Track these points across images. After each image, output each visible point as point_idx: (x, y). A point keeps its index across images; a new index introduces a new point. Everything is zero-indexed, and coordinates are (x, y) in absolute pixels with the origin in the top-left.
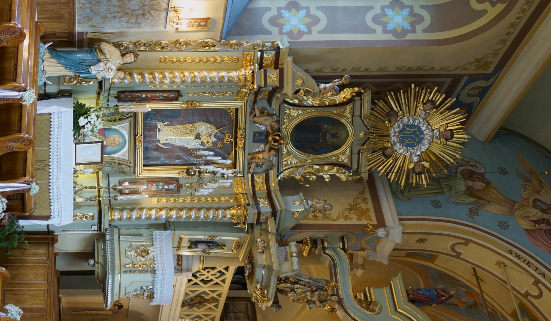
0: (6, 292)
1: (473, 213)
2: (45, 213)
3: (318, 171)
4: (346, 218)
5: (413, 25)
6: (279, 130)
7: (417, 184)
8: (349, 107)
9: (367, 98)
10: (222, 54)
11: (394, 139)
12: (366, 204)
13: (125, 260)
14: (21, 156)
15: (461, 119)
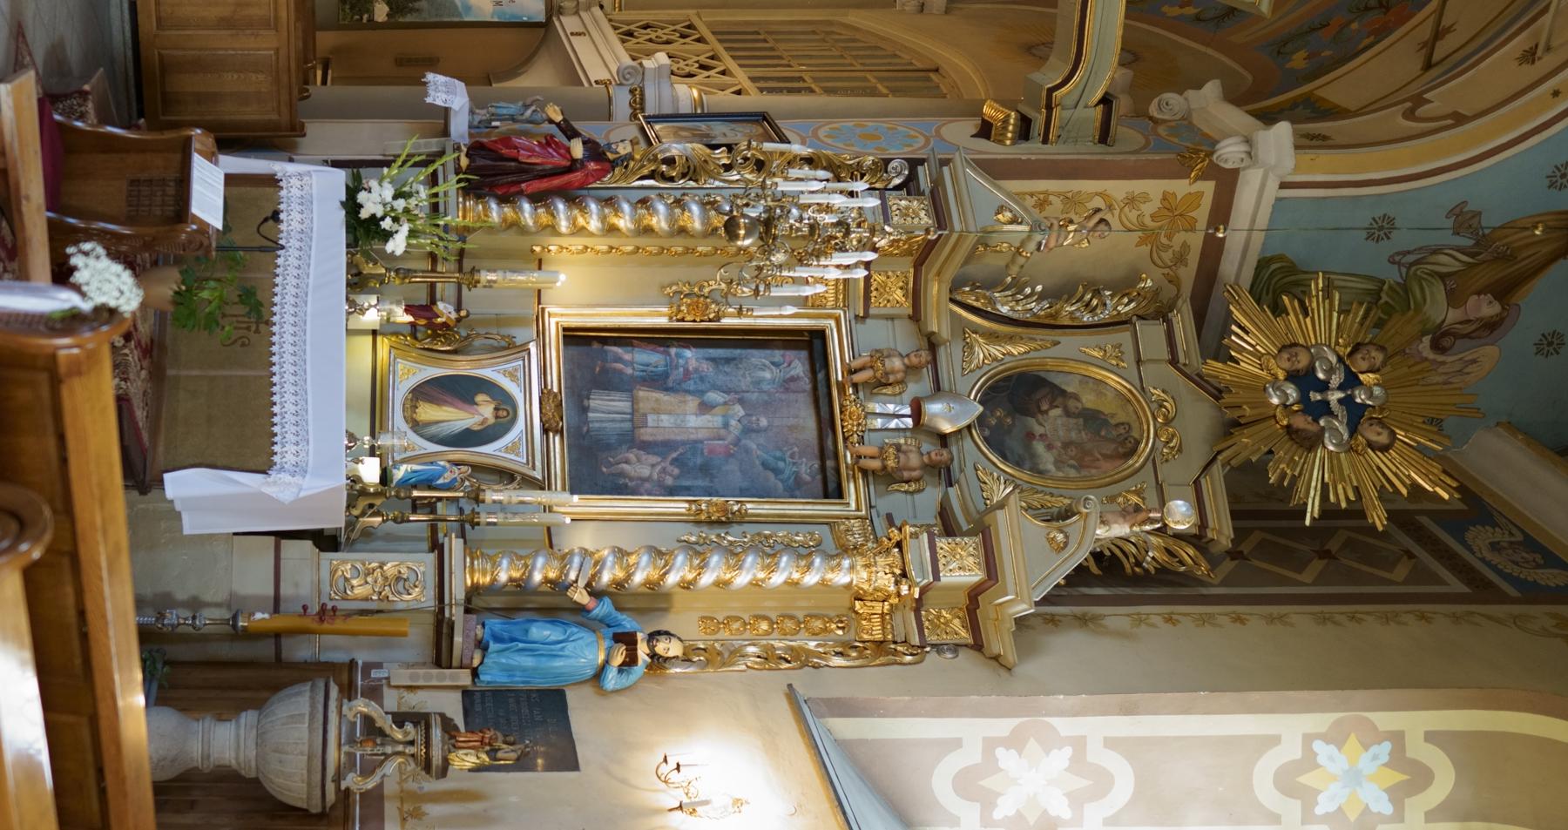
0: (807, 468)
5: (990, 764)
14: (152, 700)
15: (1365, 317)
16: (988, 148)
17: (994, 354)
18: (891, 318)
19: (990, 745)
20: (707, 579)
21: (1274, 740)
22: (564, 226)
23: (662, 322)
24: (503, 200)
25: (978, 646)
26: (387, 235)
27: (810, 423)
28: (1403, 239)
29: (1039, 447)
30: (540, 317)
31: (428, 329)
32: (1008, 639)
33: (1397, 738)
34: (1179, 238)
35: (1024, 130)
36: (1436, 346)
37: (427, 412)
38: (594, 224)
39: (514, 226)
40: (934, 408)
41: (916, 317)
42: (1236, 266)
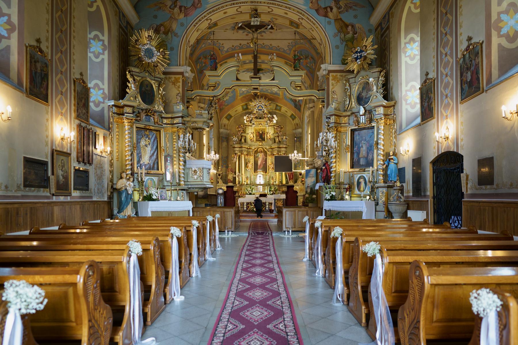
0: (370, 131)
1: (178, 37)
2: (187, 213)
3: (161, 95)
4: (179, 87)
5: (100, 40)
6: (146, 110)
7: (168, 56)
8: (136, 78)
9: (133, 69)
10: (115, 131)
11: (150, 61)
16: (325, 107)
17: (354, 103)
18: (349, 119)
19: (407, 104)
21: (406, 62)
22: (335, 169)
23: (350, 154)
25: (394, 106)
26: (332, 195)
28: (339, 43)
29: (367, 96)
30: (349, 172)
32: (391, 102)
33: (405, 43)
34: (338, 77)
35: (323, 101)
36: (356, 34)
37: (362, 189)
38: (334, 165)
39: (335, 176)
40: (361, 114)
41: (349, 116)
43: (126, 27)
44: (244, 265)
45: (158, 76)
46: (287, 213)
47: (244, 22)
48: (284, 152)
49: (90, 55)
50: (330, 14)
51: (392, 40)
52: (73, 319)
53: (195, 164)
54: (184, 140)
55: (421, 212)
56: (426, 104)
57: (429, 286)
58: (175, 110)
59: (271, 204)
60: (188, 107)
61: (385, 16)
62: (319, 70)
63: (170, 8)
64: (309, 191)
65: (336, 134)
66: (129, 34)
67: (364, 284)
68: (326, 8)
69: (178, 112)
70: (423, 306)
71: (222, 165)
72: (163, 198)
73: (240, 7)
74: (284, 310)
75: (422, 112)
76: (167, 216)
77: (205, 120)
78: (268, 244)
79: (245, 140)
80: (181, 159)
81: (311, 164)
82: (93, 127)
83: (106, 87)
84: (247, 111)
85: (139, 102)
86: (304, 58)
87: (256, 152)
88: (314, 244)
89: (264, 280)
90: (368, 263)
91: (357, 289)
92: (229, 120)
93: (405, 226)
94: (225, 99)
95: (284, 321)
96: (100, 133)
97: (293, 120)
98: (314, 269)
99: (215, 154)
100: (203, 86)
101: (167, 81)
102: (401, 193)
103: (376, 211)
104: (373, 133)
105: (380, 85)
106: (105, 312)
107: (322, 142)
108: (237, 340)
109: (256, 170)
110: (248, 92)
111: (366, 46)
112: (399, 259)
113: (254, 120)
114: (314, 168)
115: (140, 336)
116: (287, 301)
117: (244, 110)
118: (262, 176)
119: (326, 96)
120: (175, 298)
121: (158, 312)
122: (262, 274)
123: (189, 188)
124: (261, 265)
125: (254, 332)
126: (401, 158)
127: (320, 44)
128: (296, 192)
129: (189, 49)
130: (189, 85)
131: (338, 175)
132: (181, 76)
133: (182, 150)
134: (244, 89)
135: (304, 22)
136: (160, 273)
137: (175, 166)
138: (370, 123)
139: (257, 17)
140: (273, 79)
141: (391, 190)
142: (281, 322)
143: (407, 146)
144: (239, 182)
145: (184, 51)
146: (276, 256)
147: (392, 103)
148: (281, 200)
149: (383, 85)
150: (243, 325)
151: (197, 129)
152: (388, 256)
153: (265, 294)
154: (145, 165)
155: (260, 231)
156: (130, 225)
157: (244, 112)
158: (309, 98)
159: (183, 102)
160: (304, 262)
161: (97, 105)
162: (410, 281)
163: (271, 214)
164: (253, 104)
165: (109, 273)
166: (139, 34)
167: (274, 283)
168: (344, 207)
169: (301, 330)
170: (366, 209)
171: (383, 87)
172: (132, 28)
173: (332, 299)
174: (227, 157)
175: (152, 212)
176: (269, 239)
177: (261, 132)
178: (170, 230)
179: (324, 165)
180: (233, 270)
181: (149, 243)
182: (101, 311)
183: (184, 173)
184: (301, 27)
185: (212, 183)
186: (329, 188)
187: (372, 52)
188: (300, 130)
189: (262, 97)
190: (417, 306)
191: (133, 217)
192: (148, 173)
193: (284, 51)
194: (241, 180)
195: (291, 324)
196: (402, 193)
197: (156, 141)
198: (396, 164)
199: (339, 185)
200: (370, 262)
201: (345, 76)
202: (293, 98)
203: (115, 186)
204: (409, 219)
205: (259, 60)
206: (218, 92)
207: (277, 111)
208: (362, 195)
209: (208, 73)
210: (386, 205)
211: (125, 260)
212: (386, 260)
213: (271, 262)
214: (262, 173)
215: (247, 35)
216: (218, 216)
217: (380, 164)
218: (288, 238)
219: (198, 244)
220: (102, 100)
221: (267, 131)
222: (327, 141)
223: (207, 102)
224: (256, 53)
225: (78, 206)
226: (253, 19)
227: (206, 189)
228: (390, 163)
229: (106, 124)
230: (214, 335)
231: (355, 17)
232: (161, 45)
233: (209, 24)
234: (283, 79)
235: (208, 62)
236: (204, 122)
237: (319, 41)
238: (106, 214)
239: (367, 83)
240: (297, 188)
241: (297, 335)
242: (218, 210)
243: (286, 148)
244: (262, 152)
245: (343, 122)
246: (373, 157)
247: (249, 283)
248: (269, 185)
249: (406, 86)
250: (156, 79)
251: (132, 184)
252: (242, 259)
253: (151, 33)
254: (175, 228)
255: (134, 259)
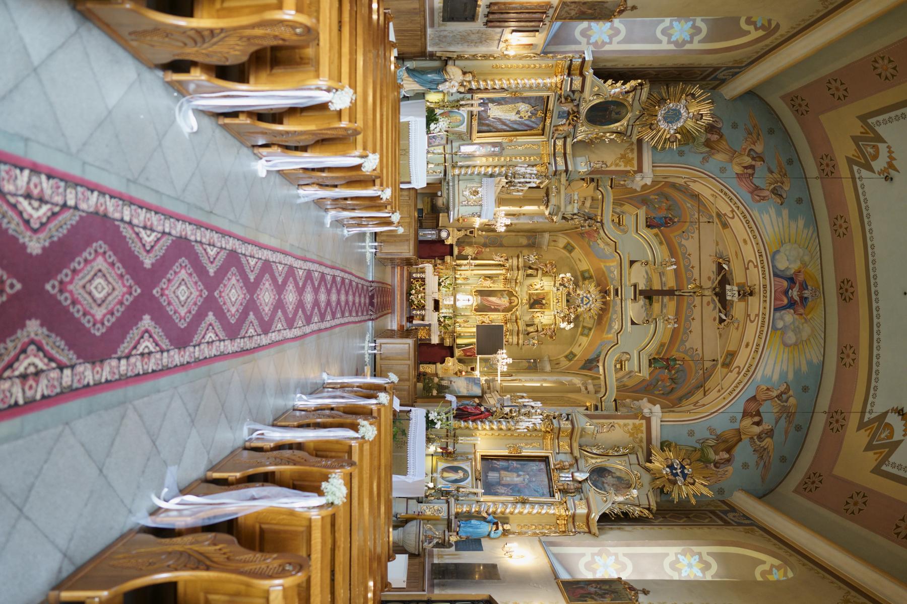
0: (546, 491)
4: (617, 165)
6: (578, 112)
8: (631, 95)
9: (646, 89)
11: (660, 117)
12: (633, 153)
13: (462, 199)
16: (589, 412)
19: (593, 555)
20: (516, 511)
21: (667, 555)
22: (480, 428)
23: (507, 454)
24: (465, 421)
25: (590, 532)
26: (436, 424)
27: (546, 480)
29: (606, 485)
30: (475, 453)
31: (446, 454)
34: (640, 435)
36: (715, 466)
37: (446, 475)
38: (487, 427)
39: (467, 428)
40: (576, 474)
41: (572, 453)
42: (656, 442)
43: (715, 79)
44: (316, 274)
45: (635, 131)
46: (405, 346)
47: (731, 274)
48: (510, 340)
49: (667, 21)
50: (748, 422)
51: (706, 530)
52: (226, 5)
53: (489, 192)
54: (529, 175)
55: (405, 579)
56: (592, 590)
57: (266, 588)
58: (579, 159)
59: (423, 320)
60: (583, 179)
61: (748, 518)
62: (650, 401)
63: (751, 150)
64: (444, 383)
65: (541, 431)
66: (704, 83)
67: (277, 476)
68: (758, 414)
69: (575, 164)
70: (233, 576)
71: (488, 236)
72: (431, 140)
73: (756, 266)
74: (238, 340)
75: (578, 582)
76: (402, 147)
77: (562, 209)
78: (354, 314)
79: (528, 276)
80: (497, 169)
81: (489, 388)
82: (547, 26)
83: (615, 46)
84: (582, 278)
85: (590, 101)
86: (671, 377)
87: (511, 294)
88: (352, 392)
89: (290, 308)
90: (312, 484)
91: (271, 465)
92: (565, 248)
93: (379, 550)
94: (599, 241)
95: (220, 340)
96: (538, 39)
97: (566, 357)
98: (309, 390)
99: (507, 226)
100: (621, 205)
101: (626, 145)
102: (437, 543)
103: (408, 499)
104: (543, 495)
105: (625, 508)
106: (237, 53)
107: (525, 406)
108: (190, 262)
109: (481, 293)
110: (613, 279)
111: (693, 484)
112: (317, 536)
113: (565, 291)
114: (484, 392)
115: (200, 108)
116: (253, 345)
117: (582, 273)
118: (470, 303)
119: (605, 413)
120: (263, 161)
121: (239, 135)
122: (300, 304)
123: (448, 183)
124: (316, 303)
125: (201, 291)
126: (499, 544)
127: (695, 404)
128: (442, 362)
129: (681, 181)
130: (622, 183)
131: (470, 433)
132: (636, 169)
133: (511, 170)
134: (616, 272)
135: (733, 375)
136: (303, 137)
137: (484, 159)
138: (560, 490)
139: (739, 295)
140: (633, 323)
141: (443, 527)
142: (217, 335)
143: (518, 555)
144: (460, 265)
145: (678, 174)
146: (332, 328)
147: (595, 529)
148: (430, 335)
149: (626, 514)
150: (215, 273)
151: (547, 195)
152: (323, 518)
153: (267, 309)
154: (485, 111)
155: (377, 301)
156: (385, 88)
157: (579, 274)
158: (603, 383)
159: (591, 173)
160: (321, 375)
161: (584, 33)
162: (275, 555)
163: (405, 319)
164: (592, 288)
165: (301, 58)
166: (704, 100)
167: (285, 324)
168: (414, 443)
169: (204, 369)
170: (410, 481)
171: (622, 513)
172: (714, 88)
173: (255, 421)
174: (501, 245)
175: (408, 124)
176: (362, 315)
177: (544, 302)
178: (374, 152)
179: (487, 410)
180: (309, 256)
181: (352, 118)
182: (238, 48)
183: (473, 173)
184: (725, 370)
185: (458, 220)
186: (447, 418)
187: (684, 495)
188: (548, 368)
189: (604, 303)
190: (233, 565)
191: (399, 93)
192: (472, 115)
193: (683, 342)
194: (463, 268)
195: (214, 352)
196: (438, 545)
197: (526, 128)
198: (489, 535)
199: (453, 435)
200: (305, 484)
201: (641, 447)
202: (602, 358)
203: (450, 62)
204: (391, 558)
205: (666, 299)
206: (609, 227)
207: (580, 329)
208: (435, 475)
209: (642, 213)
210: (419, 517)
211: (323, 82)
212: (315, 515)
213: (322, 318)
214: (475, 304)
215: (709, 278)
216: (401, 230)
217: (489, 507)
218: (363, 348)
219: (352, 198)
220: (592, 40)
221: (547, 312)
222: (528, 415)
223: (593, 211)
224: (677, 293)
225: (417, 6)
226: (736, 288)
227: (447, 210)
228: (491, 525)
229: (553, 48)
230: (199, 225)
231: (745, 466)
232: (687, 136)
233: (725, 214)
234: (633, 341)
235: (663, 213)
236: (559, 208)
237: (701, 403)
238: (406, 49)
239: (629, 486)
240: (450, 362)
241: (195, 362)
242: (412, 231)
243: (518, 344)
244: (511, 303)
245: (561, 443)
246: (502, 494)
247: (285, 282)
248: (455, 316)
249: (625, 555)
250: (630, 128)
251: (454, 90)
252: (327, 271)
253: (707, 119)
254: (378, 161)
255: (322, 97)
